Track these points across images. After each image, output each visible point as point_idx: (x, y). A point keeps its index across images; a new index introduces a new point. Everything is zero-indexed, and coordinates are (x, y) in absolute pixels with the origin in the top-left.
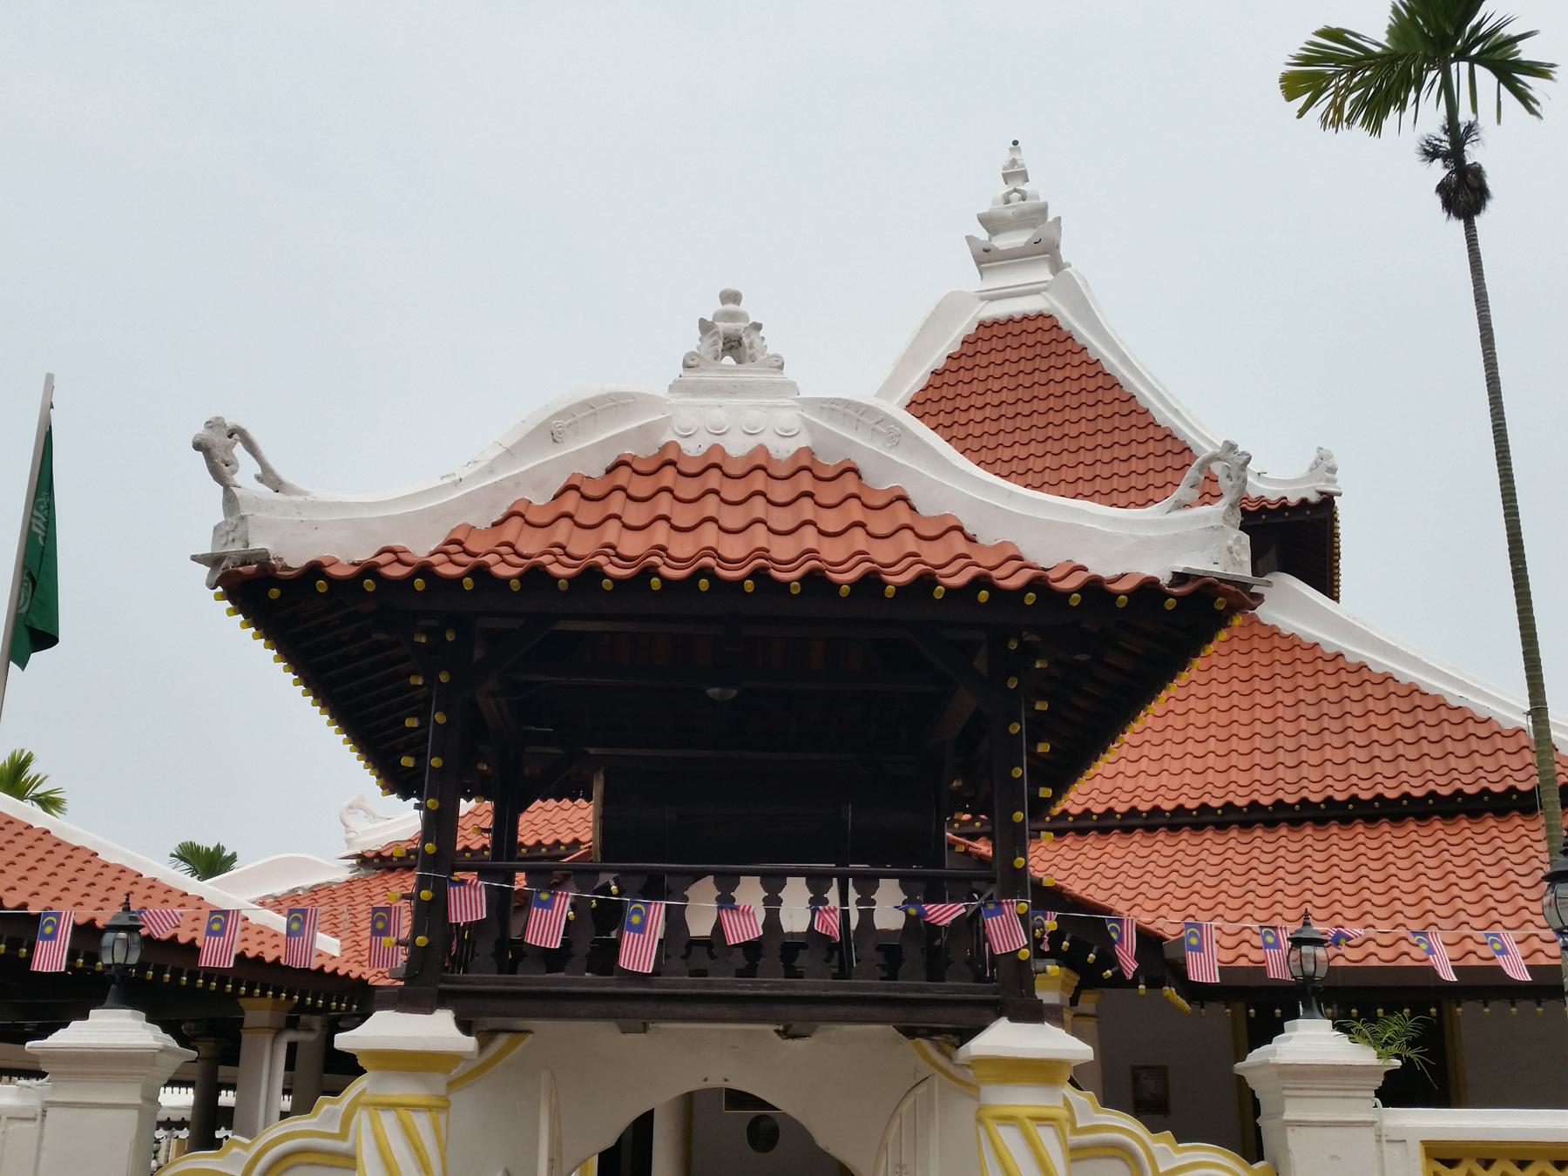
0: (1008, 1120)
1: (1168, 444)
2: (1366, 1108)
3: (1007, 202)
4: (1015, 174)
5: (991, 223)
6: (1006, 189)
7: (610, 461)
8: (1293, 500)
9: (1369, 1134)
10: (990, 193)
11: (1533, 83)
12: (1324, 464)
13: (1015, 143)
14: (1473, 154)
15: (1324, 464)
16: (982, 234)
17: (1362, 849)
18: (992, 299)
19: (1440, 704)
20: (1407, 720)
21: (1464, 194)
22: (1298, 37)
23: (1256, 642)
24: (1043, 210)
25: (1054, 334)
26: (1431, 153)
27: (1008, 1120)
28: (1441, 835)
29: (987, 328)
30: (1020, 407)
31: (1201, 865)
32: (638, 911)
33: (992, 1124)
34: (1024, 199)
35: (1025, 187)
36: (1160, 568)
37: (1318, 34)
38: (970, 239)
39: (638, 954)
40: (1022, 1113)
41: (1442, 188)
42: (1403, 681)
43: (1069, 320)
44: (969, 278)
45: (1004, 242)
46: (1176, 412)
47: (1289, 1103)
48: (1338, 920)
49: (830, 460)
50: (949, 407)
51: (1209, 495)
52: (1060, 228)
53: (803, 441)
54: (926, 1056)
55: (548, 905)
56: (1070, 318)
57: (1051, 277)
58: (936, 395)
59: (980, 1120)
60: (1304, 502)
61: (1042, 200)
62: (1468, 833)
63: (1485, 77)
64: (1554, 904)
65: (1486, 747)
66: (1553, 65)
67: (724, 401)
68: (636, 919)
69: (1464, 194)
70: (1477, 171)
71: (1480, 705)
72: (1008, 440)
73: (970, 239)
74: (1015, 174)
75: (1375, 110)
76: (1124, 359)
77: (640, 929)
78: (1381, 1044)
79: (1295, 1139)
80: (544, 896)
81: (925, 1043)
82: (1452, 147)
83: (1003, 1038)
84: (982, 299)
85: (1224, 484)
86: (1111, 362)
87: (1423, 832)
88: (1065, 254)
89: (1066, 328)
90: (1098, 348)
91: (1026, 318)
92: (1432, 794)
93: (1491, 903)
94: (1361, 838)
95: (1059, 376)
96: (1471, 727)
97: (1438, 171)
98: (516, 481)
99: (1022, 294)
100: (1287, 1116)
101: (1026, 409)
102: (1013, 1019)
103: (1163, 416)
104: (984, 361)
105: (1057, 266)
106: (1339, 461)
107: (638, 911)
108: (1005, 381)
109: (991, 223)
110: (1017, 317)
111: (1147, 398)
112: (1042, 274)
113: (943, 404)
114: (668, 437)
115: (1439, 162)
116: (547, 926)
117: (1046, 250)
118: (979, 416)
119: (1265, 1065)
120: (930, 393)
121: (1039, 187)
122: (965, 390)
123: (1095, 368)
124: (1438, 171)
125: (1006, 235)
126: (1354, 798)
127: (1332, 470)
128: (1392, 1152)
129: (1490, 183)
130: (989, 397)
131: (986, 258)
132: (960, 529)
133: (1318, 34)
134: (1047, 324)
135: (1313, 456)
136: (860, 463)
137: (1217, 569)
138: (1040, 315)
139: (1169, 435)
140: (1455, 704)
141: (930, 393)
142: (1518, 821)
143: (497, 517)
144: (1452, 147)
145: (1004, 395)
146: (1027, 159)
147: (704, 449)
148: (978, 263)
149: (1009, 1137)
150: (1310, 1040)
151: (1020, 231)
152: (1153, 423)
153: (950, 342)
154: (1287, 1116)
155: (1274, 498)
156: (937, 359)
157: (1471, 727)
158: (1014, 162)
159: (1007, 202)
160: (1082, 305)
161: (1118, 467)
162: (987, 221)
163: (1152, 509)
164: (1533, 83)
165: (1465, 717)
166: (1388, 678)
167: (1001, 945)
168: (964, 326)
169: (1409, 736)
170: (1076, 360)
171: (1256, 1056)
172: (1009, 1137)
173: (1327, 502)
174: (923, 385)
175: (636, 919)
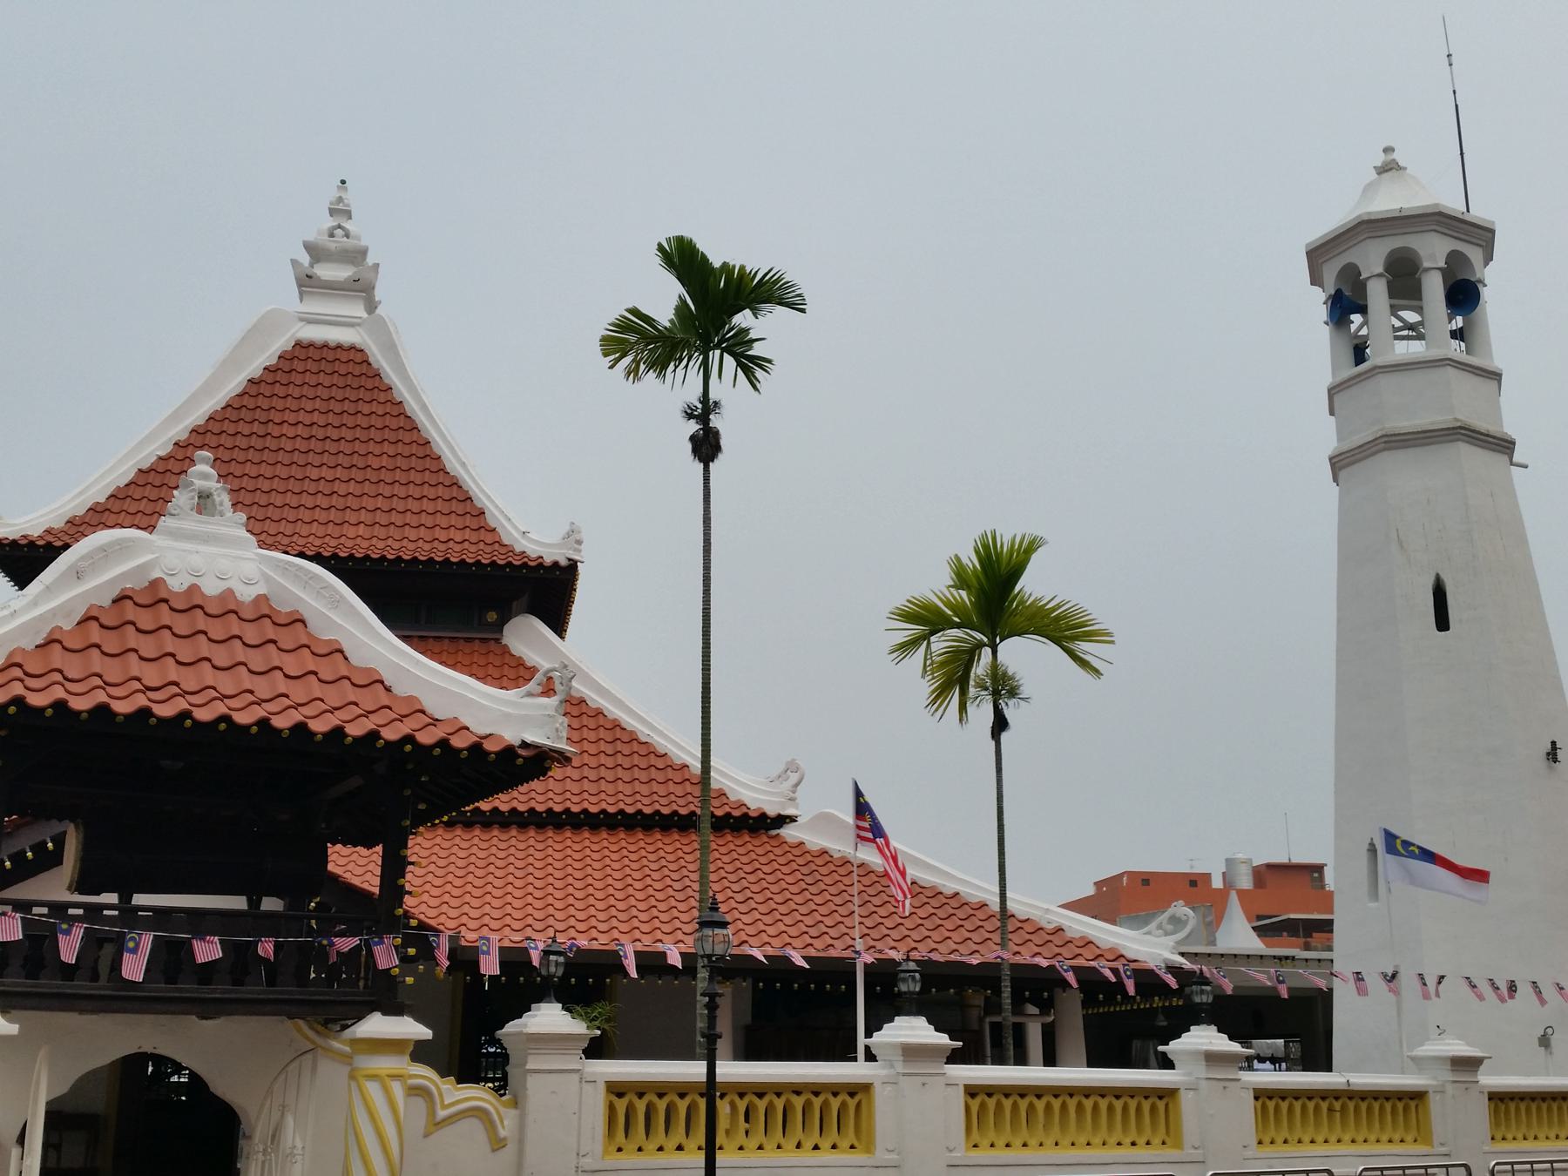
0: (374, 1077)
1: (455, 492)
2: (575, 1061)
3: (332, 235)
4: (340, 210)
5: (316, 252)
6: (331, 222)
7: (115, 593)
8: (548, 560)
9: (576, 1077)
10: (317, 225)
11: (759, 373)
12: (573, 536)
13: (343, 182)
14: (715, 421)
15: (573, 536)
16: (305, 259)
17: (569, 851)
18: (310, 322)
19: (634, 738)
20: (609, 749)
21: (706, 446)
22: (617, 311)
23: (506, 670)
24: (363, 253)
25: (364, 368)
26: (690, 415)
27: (374, 1077)
28: (623, 843)
29: (303, 349)
30: (330, 432)
31: (453, 858)
32: (133, 939)
33: (362, 1080)
34: (347, 236)
35: (347, 225)
36: (512, 735)
37: (629, 311)
38: (294, 263)
39: (134, 968)
40: (383, 1073)
41: (693, 438)
42: (610, 717)
43: (379, 358)
44: (287, 296)
45: (326, 272)
46: (463, 464)
47: (530, 1058)
48: (572, 933)
49: (283, 607)
50: (263, 417)
51: (548, 691)
52: (377, 272)
53: (261, 589)
54: (299, 1030)
55: (68, 932)
56: (380, 357)
57: (365, 315)
58: (251, 403)
59: (352, 1077)
60: (556, 564)
61: (363, 243)
62: (642, 844)
63: (729, 361)
64: (701, 939)
65: (660, 777)
66: (769, 361)
67: (202, 548)
68: (131, 945)
69: (706, 446)
70: (716, 434)
71: (661, 744)
72: (317, 460)
73: (294, 263)
74: (340, 210)
75: (660, 365)
76: (424, 407)
77: (134, 951)
78: (590, 1020)
79: (532, 1082)
80: (64, 926)
81: (301, 1022)
82: (704, 411)
83: (376, 1025)
84: (302, 320)
85: (558, 687)
86: (412, 407)
87: (613, 840)
88: (379, 294)
89: (375, 365)
90: (402, 391)
91: (339, 347)
92: (622, 812)
93: (654, 903)
94: (569, 842)
95: (366, 409)
96: (653, 760)
97: (694, 427)
98: (53, 613)
99: (338, 323)
100: (528, 1067)
101: (335, 434)
102: (385, 1013)
103: (453, 465)
104: (298, 379)
105: (371, 306)
106: (584, 536)
107: (133, 939)
108: (318, 404)
109: (316, 252)
110: (332, 344)
111: (440, 447)
112: (357, 310)
113: (258, 414)
114: (157, 574)
115: (693, 421)
116: (69, 948)
117: (362, 289)
118: (291, 432)
119: (520, 1034)
120: (246, 400)
121: (362, 228)
122: (280, 404)
123: (397, 409)
124: (694, 427)
125: (329, 265)
126: (567, 811)
127: (579, 542)
128: (588, 1088)
129: (723, 443)
130: (302, 416)
131: (307, 283)
132: (382, 682)
133: (629, 311)
134: (358, 358)
135: (567, 528)
136: (307, 616)
137: (548, 743)
138: (352, 348)
139: (455, 484)
140: (643, 739)
141: (246, 400)
142: (676, 837)
143: (40, 641)
144: (704, 411)
145: (316, 417)
146: (353, 199)
147: (185, 587)
148: (300, 285)
149: (373, 1089)
150: (548, 1018)
151: (339, 267)
152: (443, 470)
153: (267, 355)
154: (528, 1067)
155: (534, 556)
156: (254, 368)
157: (653, 760)
158: (340, 200)
159: (332, 235)
160: (391, 348)
161: (411, 504)
162: (309, 247)
163: (512, 694)
164: (759, 373)
165: (650, 751)
166: (599, 713)
167: (382, 964)
168: (281, 343)
169: (610, 762)
170: (382, 397)
171: (511, 1027)
172: (373, 1089)
173: (572, 568)
174: (239, 390)
175: (131, 945)
